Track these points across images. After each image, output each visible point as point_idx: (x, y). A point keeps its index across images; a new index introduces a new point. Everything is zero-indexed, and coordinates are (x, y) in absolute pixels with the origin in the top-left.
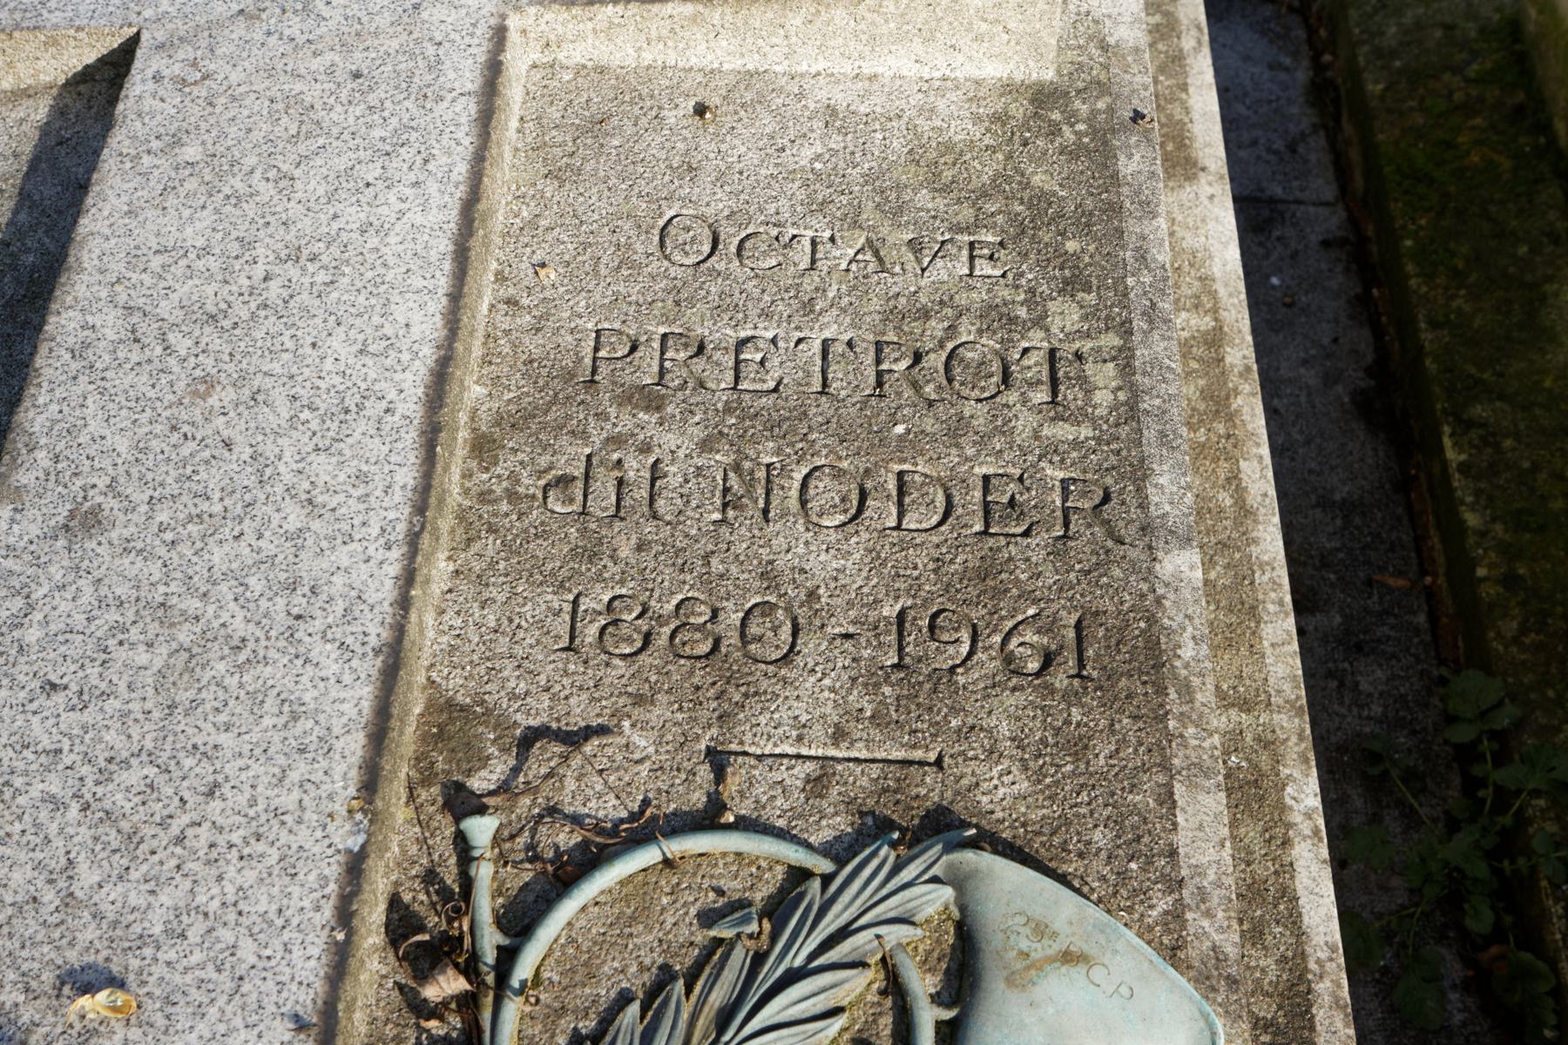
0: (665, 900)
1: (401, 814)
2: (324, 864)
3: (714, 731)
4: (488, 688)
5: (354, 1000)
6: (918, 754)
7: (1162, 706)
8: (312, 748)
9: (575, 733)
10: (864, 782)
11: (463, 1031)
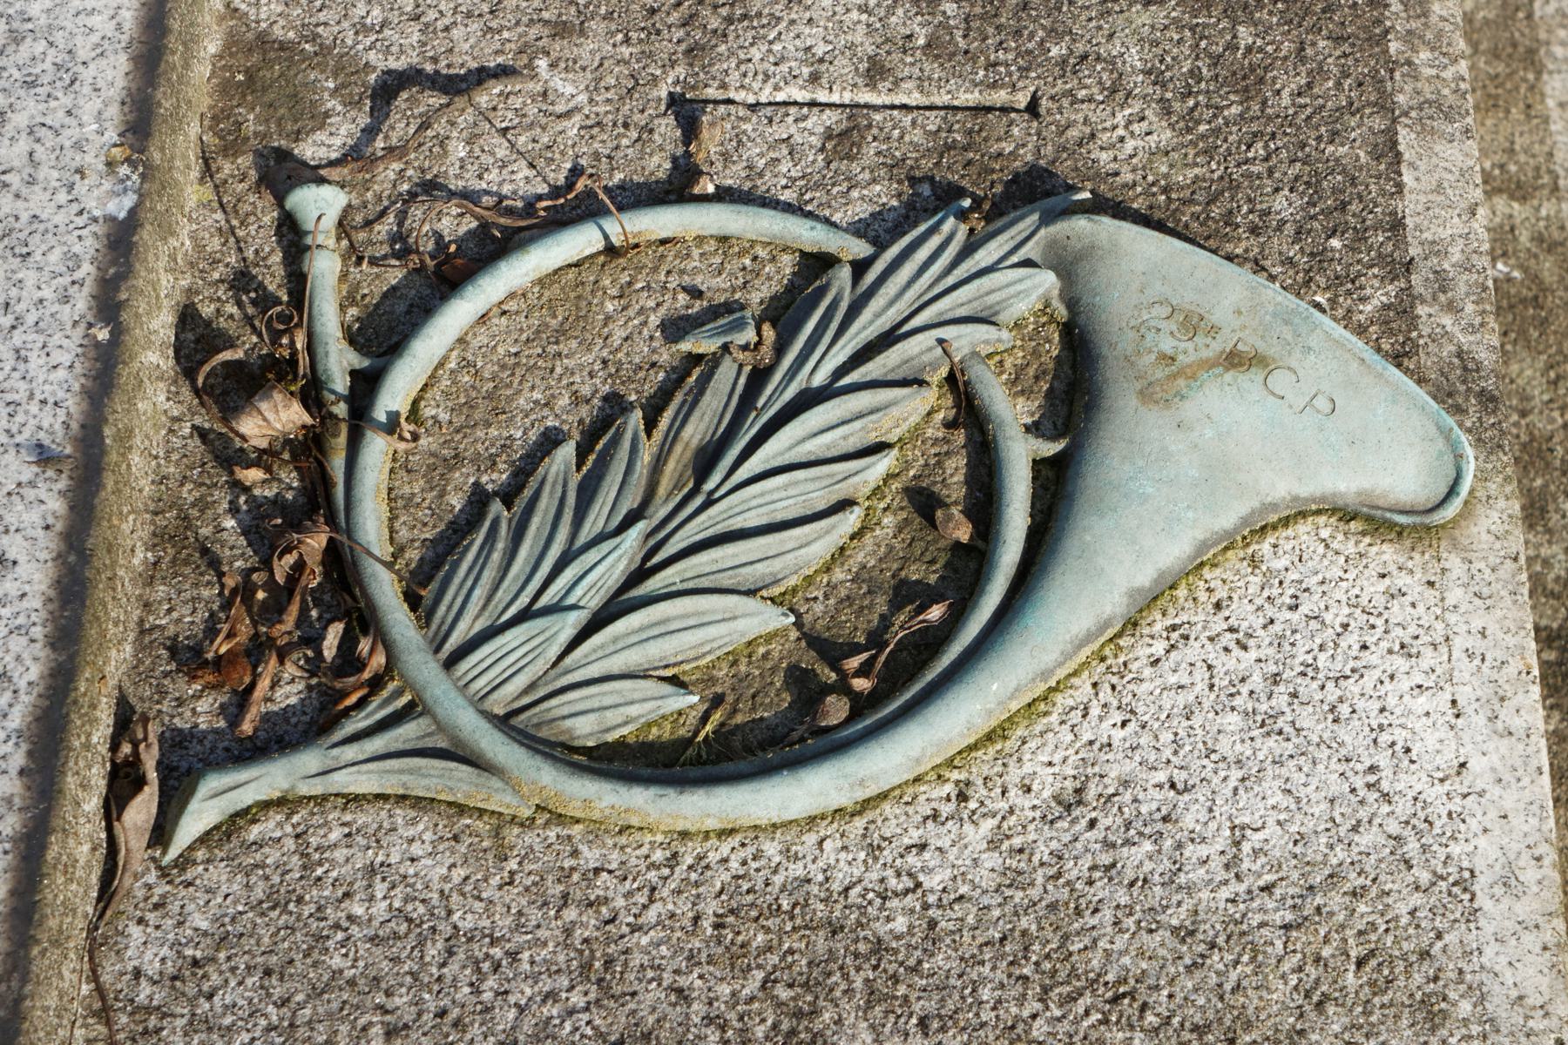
0: (610, 307)
1: (194, 193)
2: (73, 238)
3: (681, 71)
4: (322, 17)
5: (130, 433)
6: (1000, 97)
7: (1378, 22)
8: (45, 79)
9: (463, 78)
10: (917, 136)
11: (302, 491)
